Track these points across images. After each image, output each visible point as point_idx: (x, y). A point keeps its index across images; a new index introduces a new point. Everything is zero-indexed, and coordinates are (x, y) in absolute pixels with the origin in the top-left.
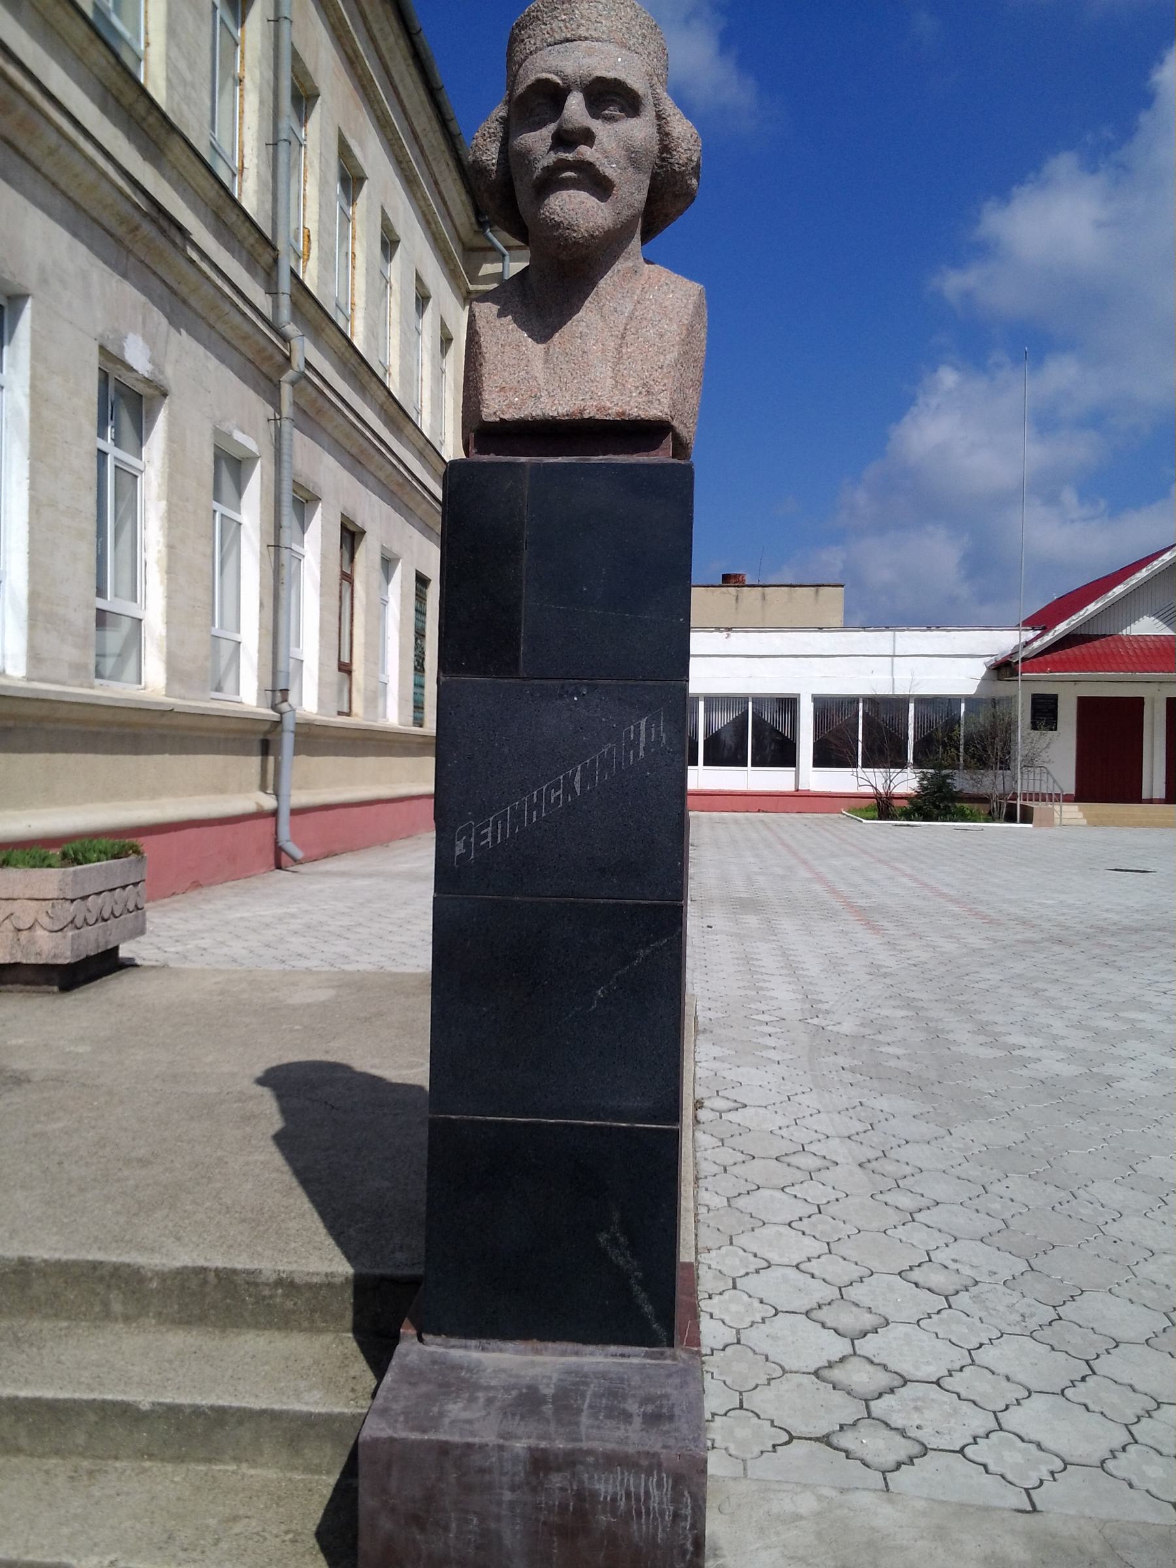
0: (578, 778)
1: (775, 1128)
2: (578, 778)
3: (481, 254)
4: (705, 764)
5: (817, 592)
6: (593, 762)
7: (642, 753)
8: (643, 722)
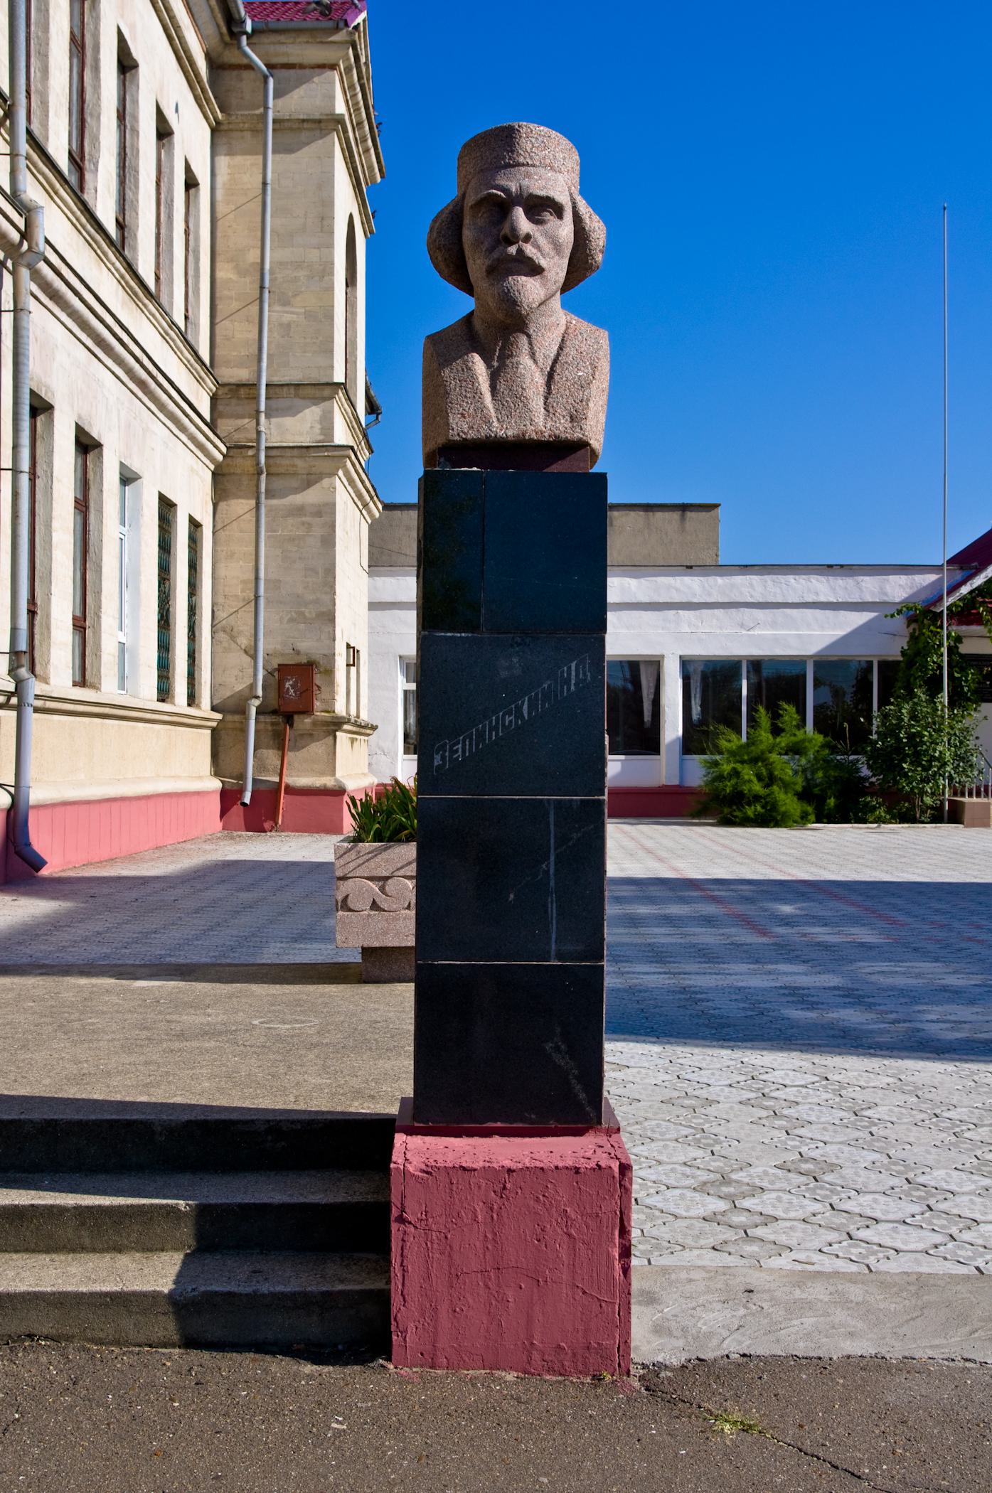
0: (525, 706)
1: (659, 1083)
2: (525, 706)
3: (235, 73)
4: (656, 664)
5: (683, 518)
6: (537, 694)
7: (573, 687)
8: (573, 665)
